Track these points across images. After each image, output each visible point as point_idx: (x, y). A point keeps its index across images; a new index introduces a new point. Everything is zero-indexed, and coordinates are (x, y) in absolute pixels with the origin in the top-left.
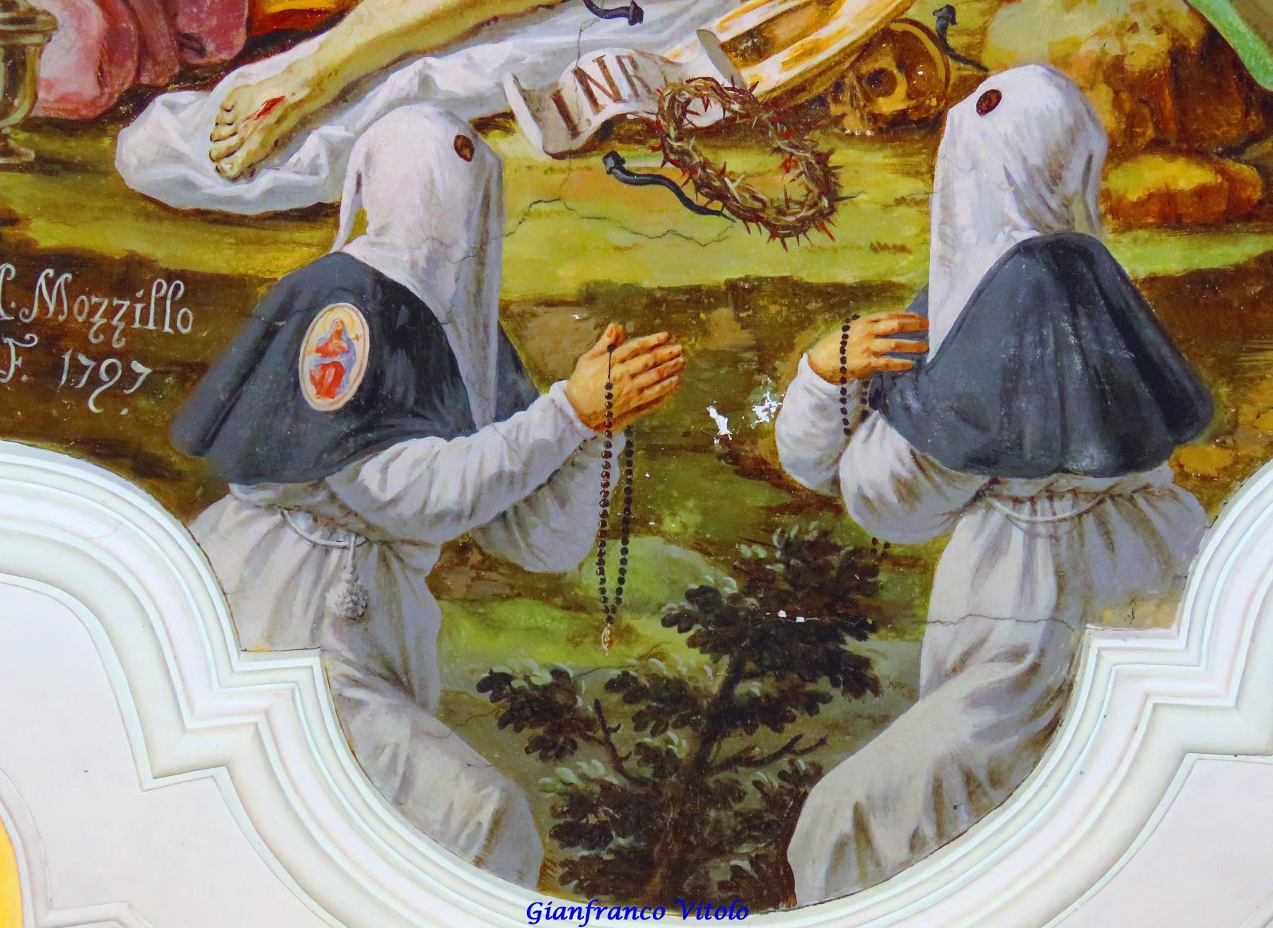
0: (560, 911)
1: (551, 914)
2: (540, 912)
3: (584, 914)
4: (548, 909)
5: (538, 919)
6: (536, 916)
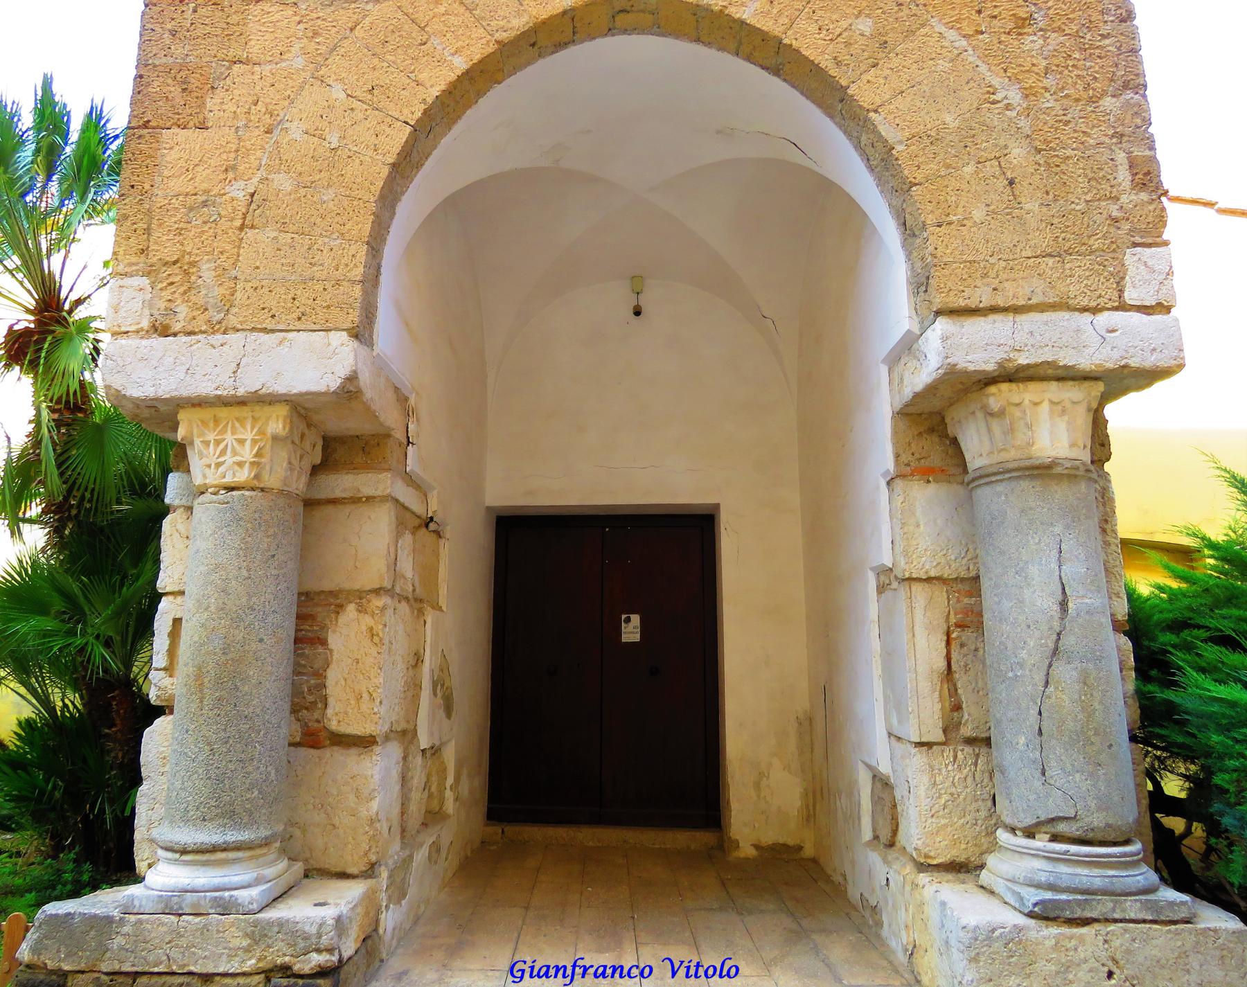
0: (601, 970)
2: (523, 971)
4: (532, 968)
5: (522, 978)
6: (519, 974)
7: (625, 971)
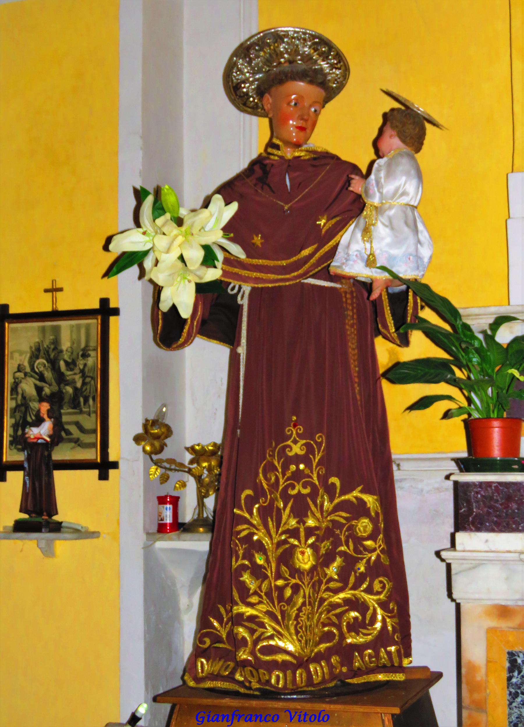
1: (210, 719)
2: (203, 718)
3: (230, 718)
4: (209, 716)
5: (203, 722)
7: (263, 719)
